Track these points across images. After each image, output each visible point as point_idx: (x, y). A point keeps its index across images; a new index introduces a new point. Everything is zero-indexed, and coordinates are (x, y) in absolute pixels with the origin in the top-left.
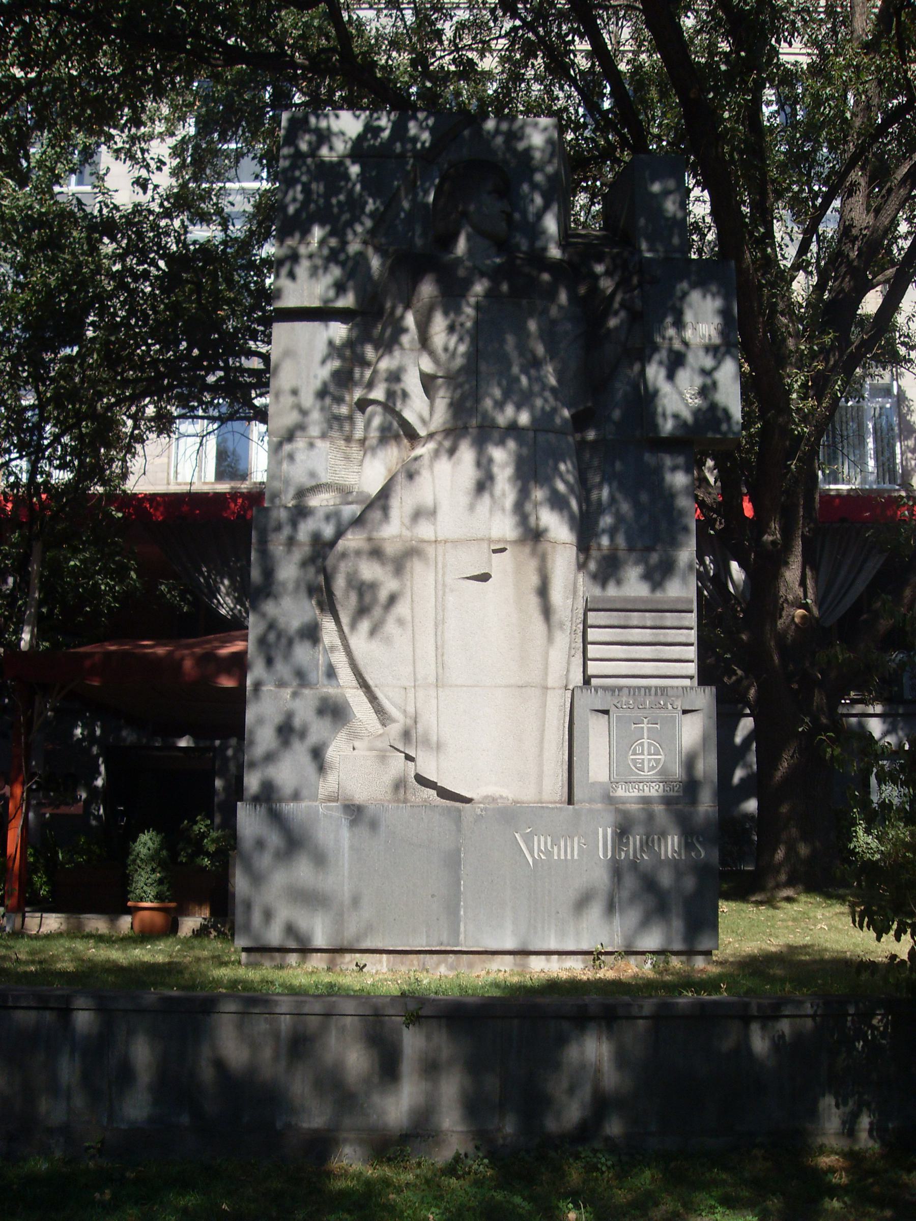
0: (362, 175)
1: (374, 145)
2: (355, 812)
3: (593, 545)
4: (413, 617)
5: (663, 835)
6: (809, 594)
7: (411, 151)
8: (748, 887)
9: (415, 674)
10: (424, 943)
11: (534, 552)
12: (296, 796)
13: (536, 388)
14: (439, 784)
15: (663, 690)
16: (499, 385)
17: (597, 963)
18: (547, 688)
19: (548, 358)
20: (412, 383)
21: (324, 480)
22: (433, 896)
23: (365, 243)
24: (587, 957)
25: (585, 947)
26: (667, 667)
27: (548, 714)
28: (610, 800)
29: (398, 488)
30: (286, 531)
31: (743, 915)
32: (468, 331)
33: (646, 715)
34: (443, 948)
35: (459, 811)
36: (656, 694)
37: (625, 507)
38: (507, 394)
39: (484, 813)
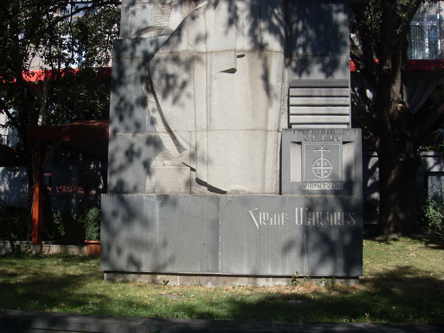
2: (165, 198)
3: (295, 54)
4: (194, 93)
5: (332, 211)
6: (404, 97)
8: (376, 232)
9: (195, 124)
10: (199, 270)
11: (260, 56)
12: (135, 190)
14: (208, 184)
15: (332, 130)
17: (294, 282)
18: (267, 131)
22: (204, 245)
24: (289, 279)
25: (287, 273)
26: (334, 118)
27: (268, 145)
28: (304, 192)
29: (186, 24)
31: (373, 248)
34: (209, 273)
35: (218, 198)
36: (328, 133)
37: (311, 32)
39: (232, 199)
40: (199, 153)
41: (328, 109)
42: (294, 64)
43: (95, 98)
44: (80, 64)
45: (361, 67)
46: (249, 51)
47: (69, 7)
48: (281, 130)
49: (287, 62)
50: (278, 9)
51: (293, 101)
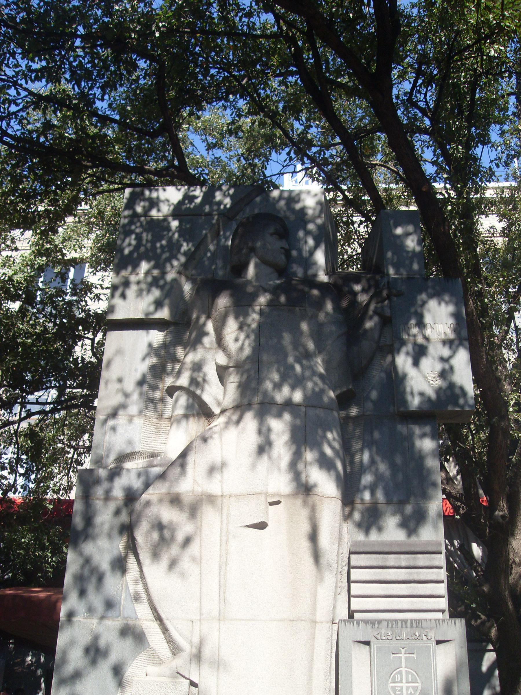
0: (180, 229)
1: (189, 207)
3: (358, 501)
7: (216, 211)
9: (201, 609)
13: (307, 373)
15: (418, 622)
16: (278, 371)
18: (315, 622)
19: (317, 352)
20: (210, 371)
21: (137, 449)
23: (179, 273)
30: (105, 485)
32: (253, 331)
33: (403, 646)
36: (412, 626)
37: (382, 467)
38: (284, 378)
40: (207, 652)
41: (411, 587)
42: (357, 516)
43: (43, 548)
44: (26, 493)
45: (461, 512)
46: (288, 496)
47: (17, 408)
48: (337, 621)
49: (346, 513)
50: (332, 432)
51: (355, 574)
